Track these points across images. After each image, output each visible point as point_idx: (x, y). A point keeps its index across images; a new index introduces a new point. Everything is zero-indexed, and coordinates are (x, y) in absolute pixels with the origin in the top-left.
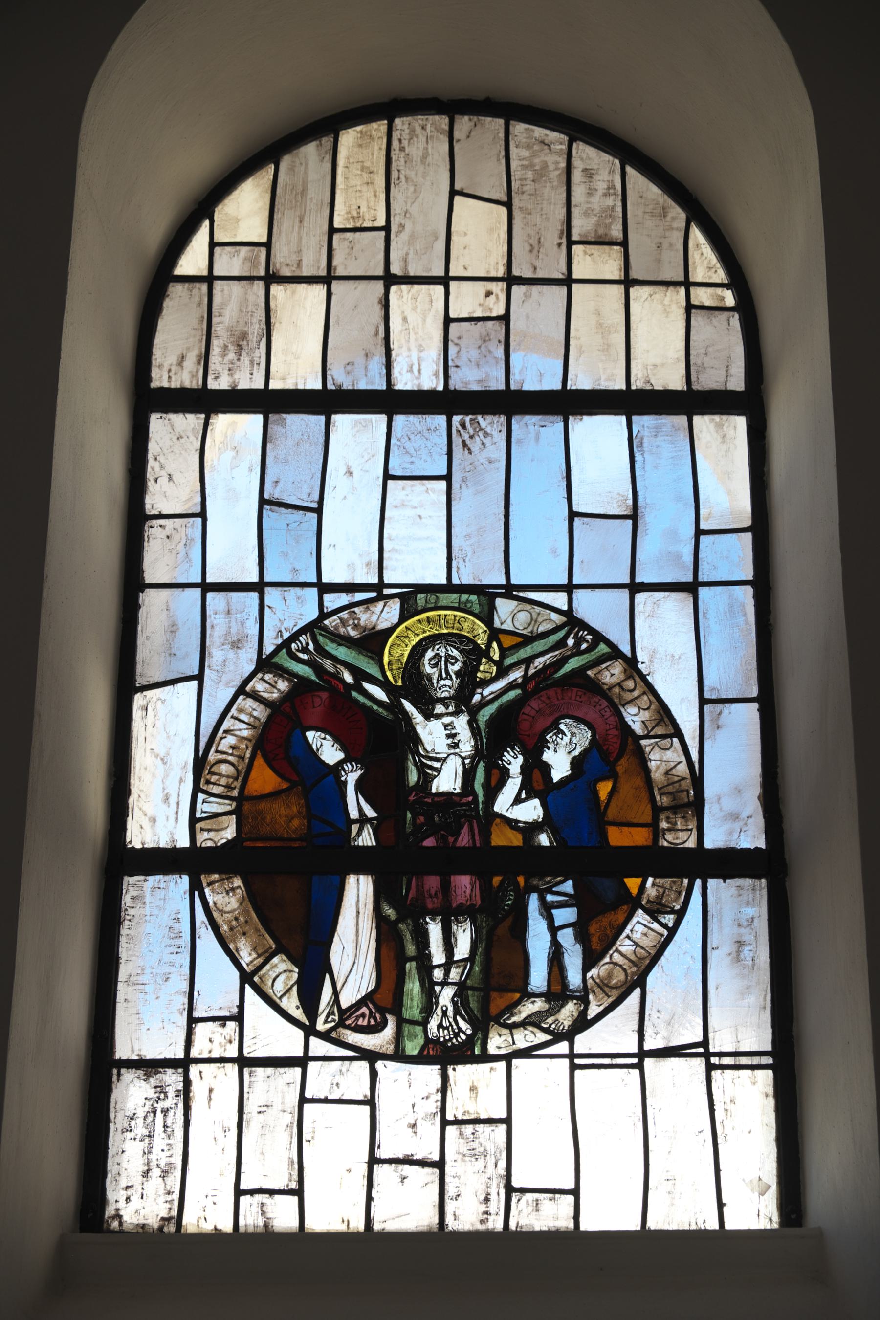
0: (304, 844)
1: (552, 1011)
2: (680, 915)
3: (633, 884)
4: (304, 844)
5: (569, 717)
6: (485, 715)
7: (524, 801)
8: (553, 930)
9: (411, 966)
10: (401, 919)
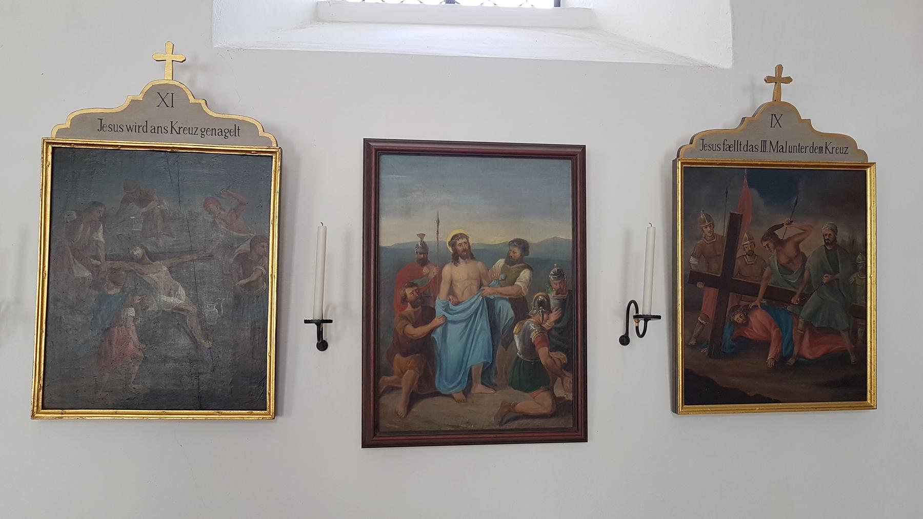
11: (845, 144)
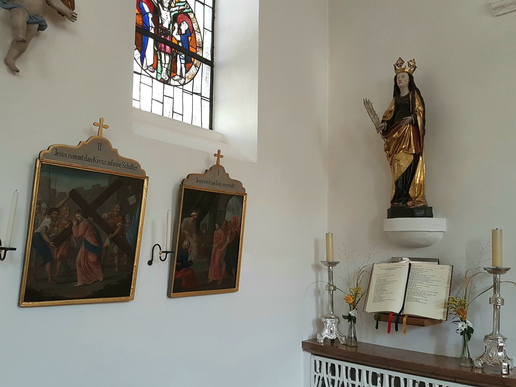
0: (142, 27)
1: (180, 80)
2: (199, 68)
3: (193, 59)
4: (142, 27)
5: (185, 21)
6: (173, 14)
7: (177, 35)
8: (181, 63)
9: (159, 61)
10: (158, 51)
11: (134, 165)
